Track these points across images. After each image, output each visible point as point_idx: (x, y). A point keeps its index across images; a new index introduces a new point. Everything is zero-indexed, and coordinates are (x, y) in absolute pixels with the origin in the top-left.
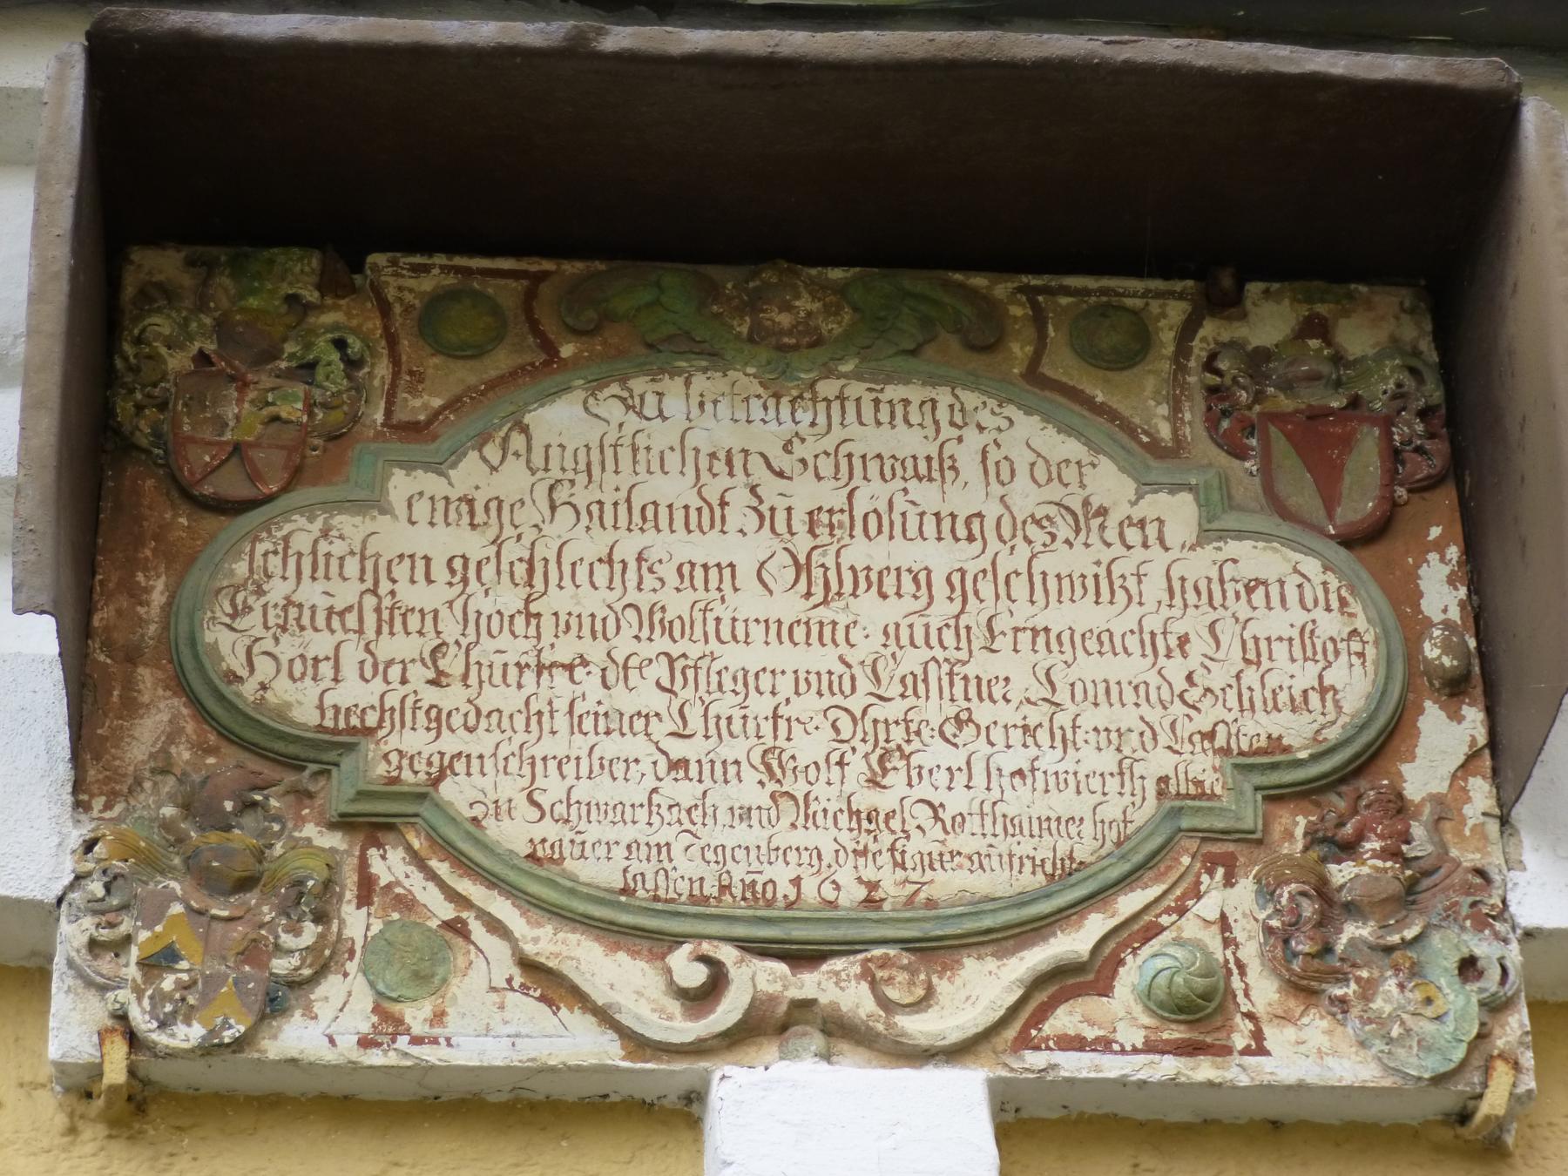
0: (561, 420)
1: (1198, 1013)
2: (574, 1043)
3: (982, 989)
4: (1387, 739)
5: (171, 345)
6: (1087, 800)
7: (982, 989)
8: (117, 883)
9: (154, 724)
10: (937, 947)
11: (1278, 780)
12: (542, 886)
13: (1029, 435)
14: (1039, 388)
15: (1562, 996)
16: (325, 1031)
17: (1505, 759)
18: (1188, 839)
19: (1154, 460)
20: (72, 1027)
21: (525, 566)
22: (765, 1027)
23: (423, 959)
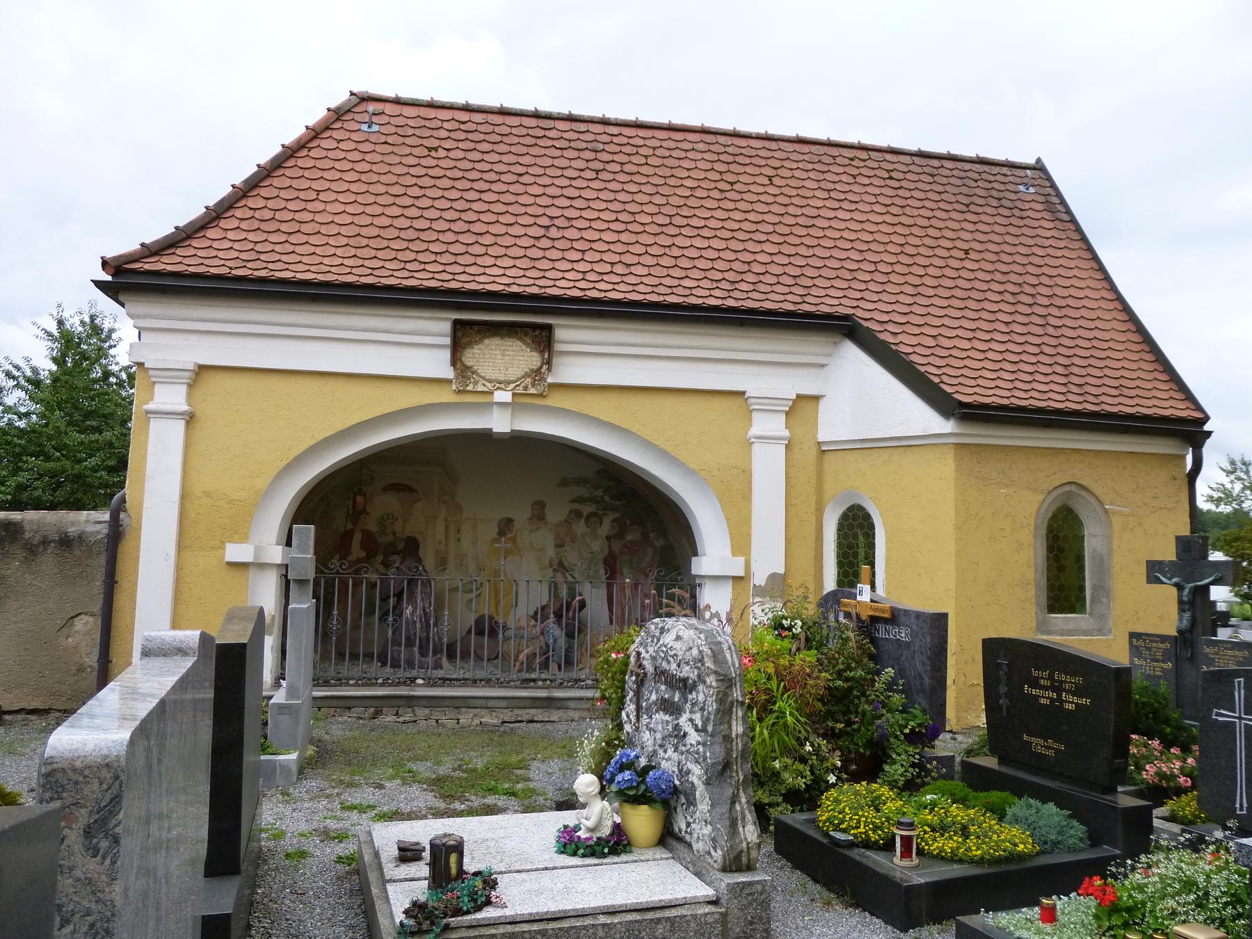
0: (486, 341)
1: (526, 388)
2: (485, 389)
3: (512, 386)
4: (541, 367)
5: (460, 334)
6: (520, 373)
7: (512, 386)
8: (457, 377)
9: (459, 365)
10: (509, 383)
11: (533, 371)
12: (483, 378)
13: (519, 343)
14: (520, 339)
15: (14, 567)
16: (470, 388)
17: (549, 370)
18: (526, 375)
19: (527, 345)
20: (454, 387)
21: (249, 558)
22: (498, 388)
23: (476, 383)
